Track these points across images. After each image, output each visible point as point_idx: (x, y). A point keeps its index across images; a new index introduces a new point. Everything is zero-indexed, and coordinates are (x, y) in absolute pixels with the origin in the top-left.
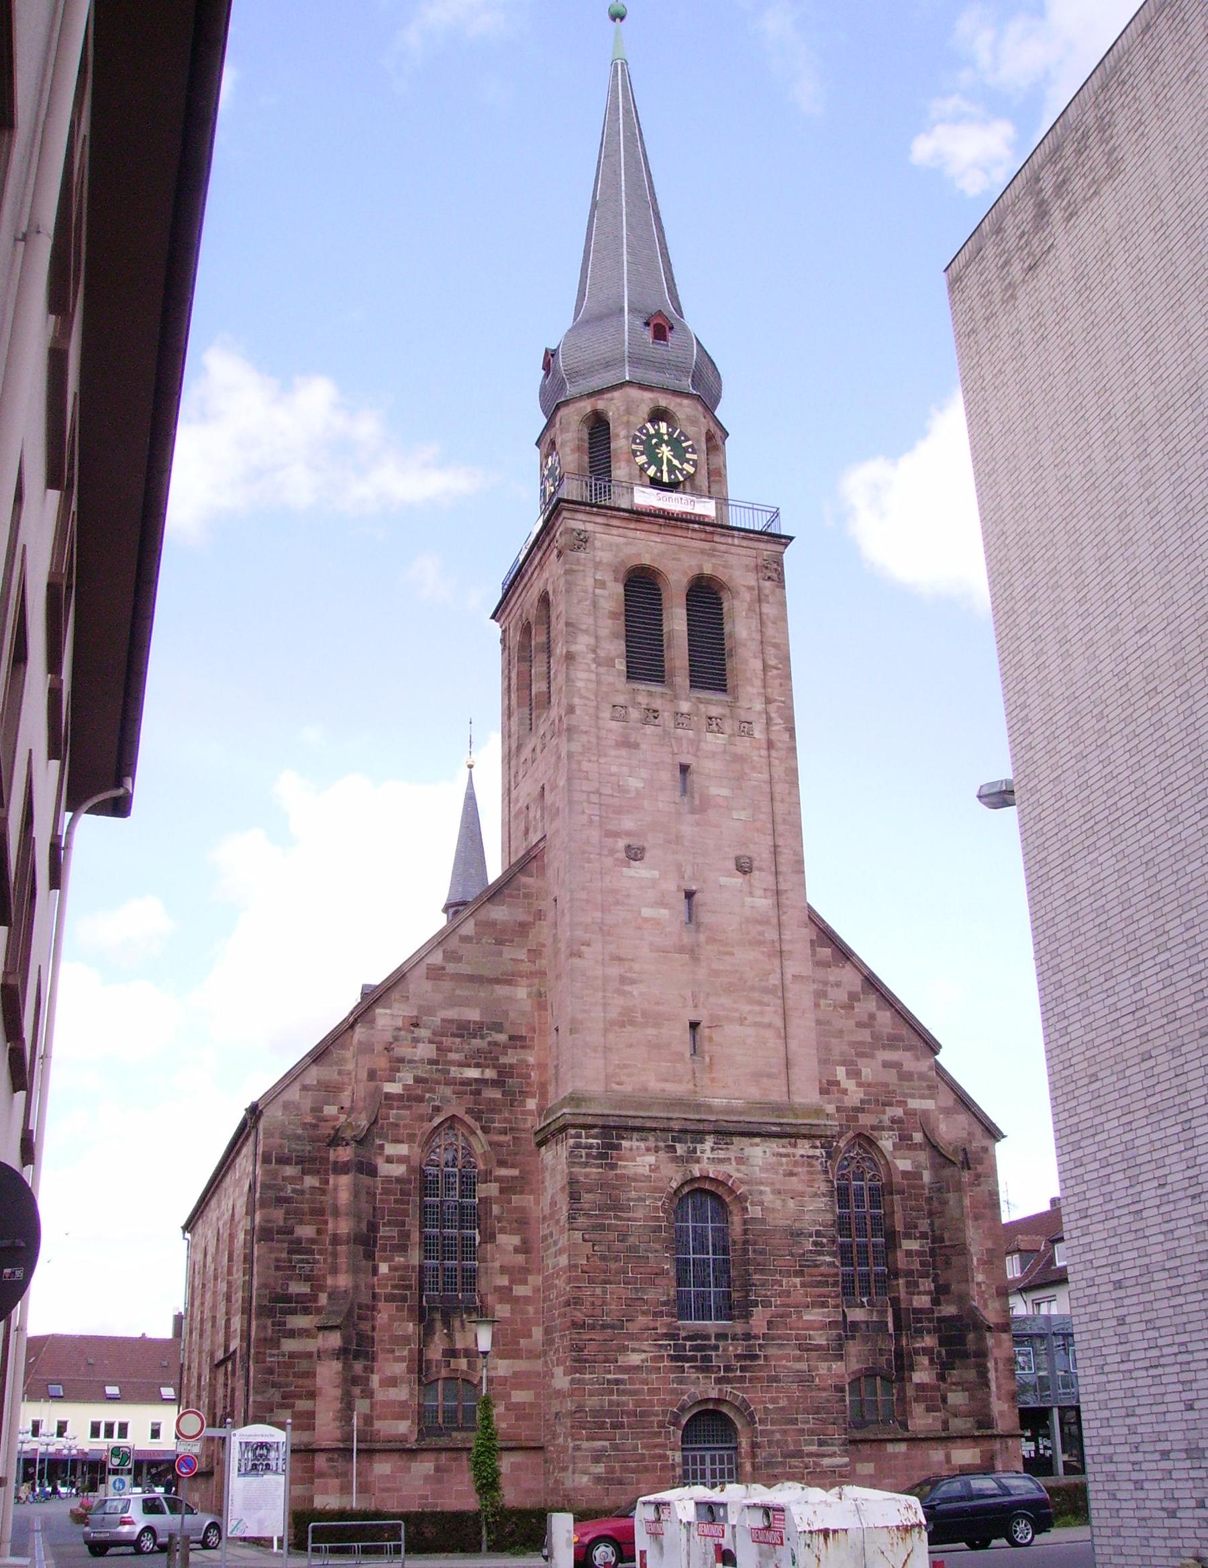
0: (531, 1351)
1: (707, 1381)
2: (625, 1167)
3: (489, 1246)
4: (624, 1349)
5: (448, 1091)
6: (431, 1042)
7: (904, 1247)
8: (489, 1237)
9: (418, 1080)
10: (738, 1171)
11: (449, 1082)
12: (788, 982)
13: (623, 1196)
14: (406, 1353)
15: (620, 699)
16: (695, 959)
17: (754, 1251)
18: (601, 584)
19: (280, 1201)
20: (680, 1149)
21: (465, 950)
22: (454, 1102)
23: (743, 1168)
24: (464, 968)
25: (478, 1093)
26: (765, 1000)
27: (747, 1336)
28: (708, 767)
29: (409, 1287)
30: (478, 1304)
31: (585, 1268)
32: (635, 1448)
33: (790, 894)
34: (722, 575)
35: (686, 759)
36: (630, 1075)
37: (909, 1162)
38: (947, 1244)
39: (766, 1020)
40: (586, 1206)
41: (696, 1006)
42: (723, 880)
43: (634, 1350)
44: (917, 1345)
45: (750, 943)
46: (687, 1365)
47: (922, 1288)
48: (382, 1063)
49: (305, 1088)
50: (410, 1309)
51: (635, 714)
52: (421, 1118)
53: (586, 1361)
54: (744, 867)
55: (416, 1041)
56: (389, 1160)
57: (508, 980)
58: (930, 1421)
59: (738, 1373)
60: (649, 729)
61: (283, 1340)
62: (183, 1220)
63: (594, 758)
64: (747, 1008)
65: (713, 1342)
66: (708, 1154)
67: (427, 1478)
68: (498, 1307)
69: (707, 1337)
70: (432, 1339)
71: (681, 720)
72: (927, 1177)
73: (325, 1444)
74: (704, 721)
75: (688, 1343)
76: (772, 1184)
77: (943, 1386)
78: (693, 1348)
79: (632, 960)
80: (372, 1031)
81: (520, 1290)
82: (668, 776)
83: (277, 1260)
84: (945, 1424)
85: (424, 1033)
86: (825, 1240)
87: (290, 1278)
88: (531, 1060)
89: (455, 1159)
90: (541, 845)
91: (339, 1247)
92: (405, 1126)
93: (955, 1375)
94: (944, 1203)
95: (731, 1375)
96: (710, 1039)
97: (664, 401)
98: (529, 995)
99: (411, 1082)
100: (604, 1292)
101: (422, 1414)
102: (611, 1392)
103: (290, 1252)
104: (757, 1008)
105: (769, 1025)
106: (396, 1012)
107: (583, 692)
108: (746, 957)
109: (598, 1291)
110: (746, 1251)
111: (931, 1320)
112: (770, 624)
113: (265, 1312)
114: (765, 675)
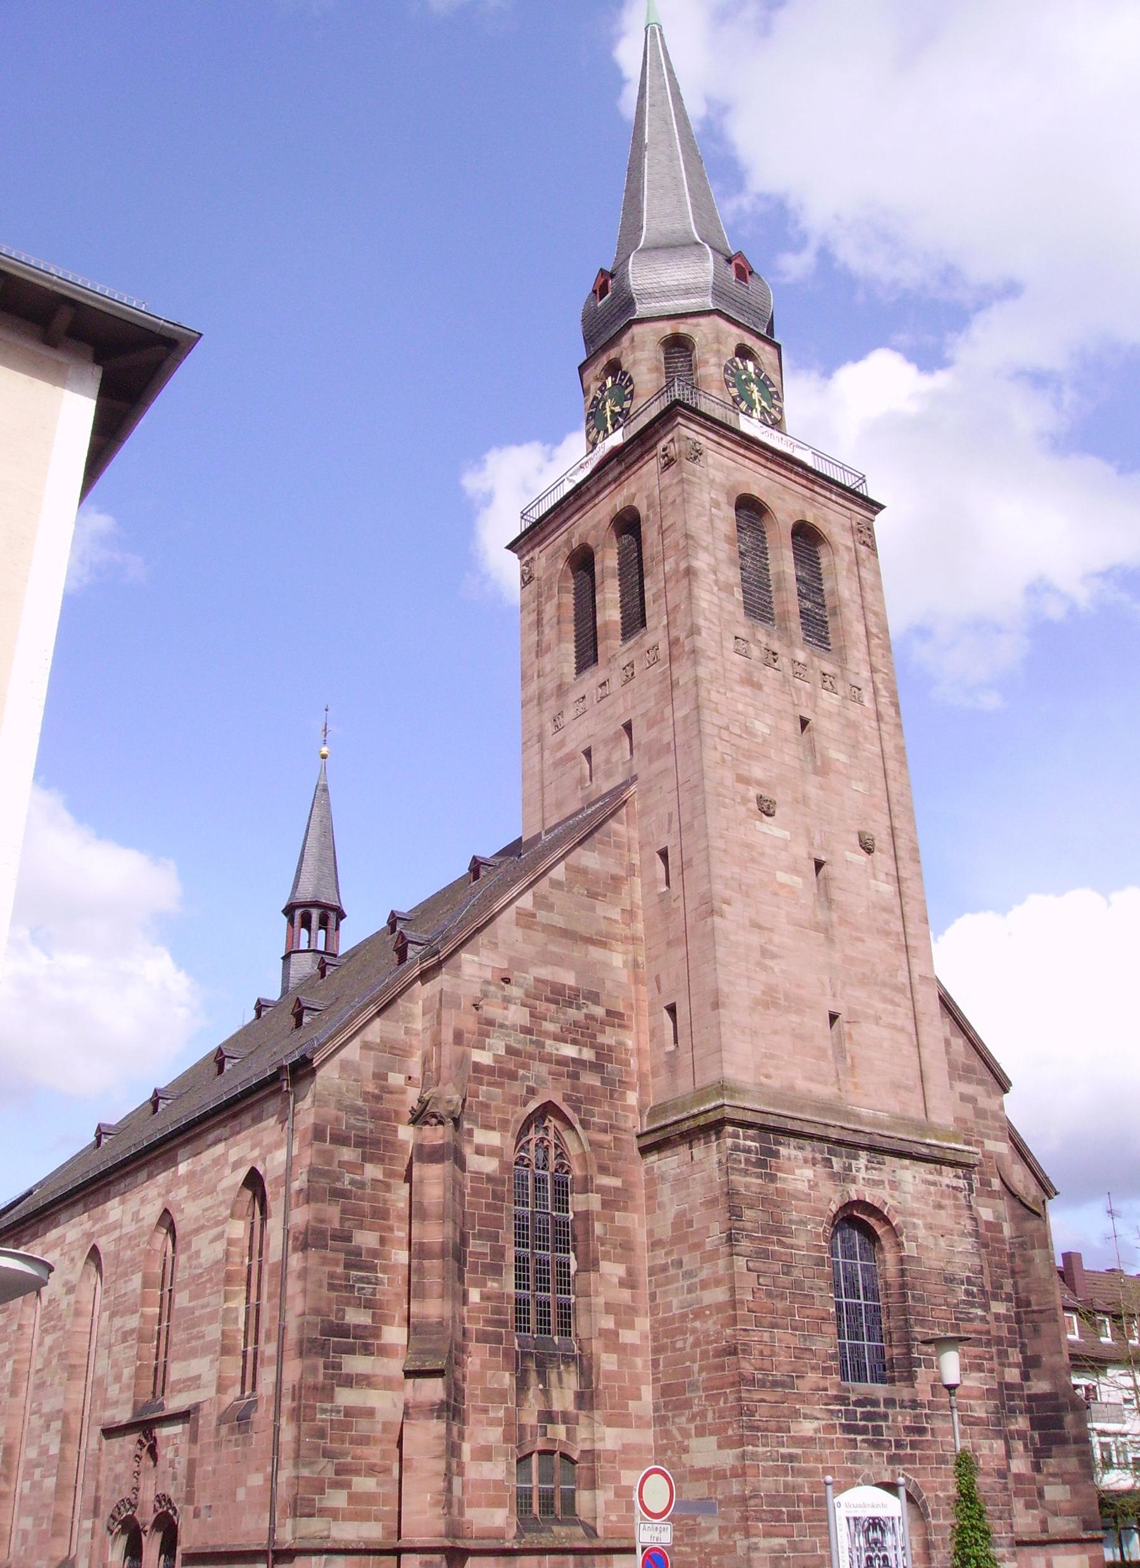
0: (639, 1418)
1: (880, 1460)
2: (784, 1180)
3: (593, 1275)
4: (796, 1414)
5: (542, 1069)
6: (524, 1005)
7: (993, 1310)
8: (590, 1264)
9: (510, 1050)
10: (892, 1196)
11: (545, 1059)
12: (916, 981)
13: (785, 1218)
14: (501, 1414)
15: (742, 632)
16: (830, 940)
17: (913, 1297)
18: (716, 504)
19: (338, 1194)
21: (556, 897)
22: (550, 1084)
23: (896, 1194)
24: (558, 921)
25: (575, 1076)
26: (896, 999)
27: (915, 1404)
28: (824, 725)
29: (503, 1323)
30: (577, 1352)
31: (751, 1305)
32: (814, 1549)
33: (909, 883)
34: (820, 525)
35: (807, 715)
36: (777, 1068)
37: (990, 1211)
38: (1035, 1308)
39: (899, 1023)
40: (749, 1225)
41: (834, 996)
42: (849, 856)
43: (806, 1417)
44: (1012, 1427)
45: (878, 931)
46: (859, 1438)
47: (1011, 1360)
48: (469, 1023)
49: (366, 1046)
50: (506, 1354)
51: (756, 652)
52: (513, 1100)
53: (758, 1429)
55: (507, 1000)
56: (479, 1151)
57: (601, 941)
58: (1030, 1520)
59: (909, 1451)
60: (770, 672)
61: (337, 1389)
63: (722, 690)
64: (880, 1006)
65: (882, 1409)
66: (863, 1174)
68: (604, 1356)
69: (875, 1403)
70: (526, 1396)
71: (799, 669)
72: (1007, 1230)
73: (419, 1541)
74: (819, 676)
75: (859, 1410)
76: (924, 1216)
77: (1038, 1477)
78: (867, 1416)
79: (771, 930)
80: (459, 981)
81: (628, 1337)
82: (790, 727)
83: (332, 1276)
84: (1044, 1522)
85: (515, 991)
86: (975, 1289)
87: (348, 1304)
88: (630, 1044)
89: (546, 1159)
91: (426, 1263)
93: (1051, 1464)
94: (1029, 1260)
95: (902, 1452)
96: (850, 1036)
97: (750, 341)
98: (625, 962)
99: (503, 1053)
100: (772, 1338)
101: (523, 1499)
102: (785, 1472)
103: (348, 1266)
104: (890, 1007)
105: (902, 1030)
106: (485, 961)
107: (707, 614)
108: (876, 946)
109: (766, 1337)
110: (904, 1296)
111: (1021, 1398)
112: (868, 590)
113: (307, 1348)
114: (868, 642)
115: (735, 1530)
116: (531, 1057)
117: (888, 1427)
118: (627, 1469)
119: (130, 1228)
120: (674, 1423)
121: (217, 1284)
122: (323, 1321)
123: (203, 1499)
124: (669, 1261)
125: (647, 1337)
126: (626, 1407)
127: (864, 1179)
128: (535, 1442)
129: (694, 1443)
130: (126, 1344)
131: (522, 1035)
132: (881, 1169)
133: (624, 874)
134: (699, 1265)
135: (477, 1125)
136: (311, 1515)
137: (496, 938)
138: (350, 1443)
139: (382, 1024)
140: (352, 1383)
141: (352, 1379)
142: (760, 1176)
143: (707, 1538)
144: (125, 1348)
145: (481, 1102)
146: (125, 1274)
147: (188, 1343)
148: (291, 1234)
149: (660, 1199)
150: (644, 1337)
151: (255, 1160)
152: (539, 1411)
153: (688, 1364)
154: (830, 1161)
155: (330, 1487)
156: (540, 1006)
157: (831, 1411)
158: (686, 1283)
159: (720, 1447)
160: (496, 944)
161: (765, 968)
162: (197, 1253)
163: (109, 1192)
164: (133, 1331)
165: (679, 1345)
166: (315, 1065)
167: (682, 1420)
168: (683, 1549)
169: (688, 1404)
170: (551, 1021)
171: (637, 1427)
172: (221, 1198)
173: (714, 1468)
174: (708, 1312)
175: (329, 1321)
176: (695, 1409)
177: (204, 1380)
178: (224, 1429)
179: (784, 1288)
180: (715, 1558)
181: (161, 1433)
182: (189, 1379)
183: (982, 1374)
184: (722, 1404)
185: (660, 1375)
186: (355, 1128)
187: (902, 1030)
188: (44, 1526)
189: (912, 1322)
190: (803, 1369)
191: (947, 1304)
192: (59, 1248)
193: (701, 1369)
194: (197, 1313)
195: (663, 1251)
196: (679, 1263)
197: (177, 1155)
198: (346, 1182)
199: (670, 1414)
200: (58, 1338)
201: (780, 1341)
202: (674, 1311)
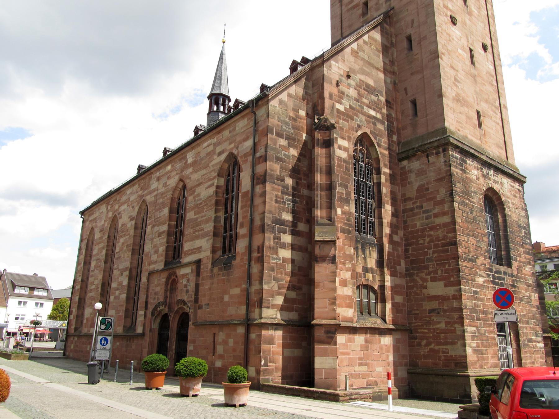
0: (400, 273)
2: (469, 173)
5: (362, 117)
6: (355, 89)
14: (350, 266)
16: (475, 80)
20: (485, 171)
21: (366, 48)
25: (375, 124)
26: (496, 112)
27: (512, 276)
41: (478, 104)
43: (480, 276)
49: (289, 95)
54: (485, 48)
55: (349, 86)
56: (340, 148)
61: (279, 249)
62: (82, 209)
64: (492, 113)
67: (361, 346)
75: (496, 275)
83: (276, 196)
85: (351, 81)
87: (284, 210)
88: (394, 115)
90: (392, 11)
92: (347, 131)
98: (391, 81)
100: (468, 240)
103: (283, 193)
104: (494, 114)
106: (340, 66)
115: (455, 322)
116: (359, 112)
117: (505, 283)
118: (396, 295)
119: (162, 190)
120: (417, 276)
121: (210, 206)
122: (273, 217)
123: (203, 301)
124: (415, 206)
125: (402, 239)
126: (396, 268)
127: (493, 179)
128: (361, 280)
129: (430, 284)
130: (160, 238)
131: (355, 102)
132: (498, 177)
133: (389, 46)
134: (432, 207)
135: (339, 136)
136: (268, 307)
137: (344, 58)
138: (285, 275)
139: (296, 87)
140: (285, 247)
141: (285, 245)
142: (461, 170)
143: (438, 326)
144: (160, 239)
145: (340, 127)
146: (160, 209)
147: (194, 233)
148: (255, 177)
149: (409, 180)
150: (401, 239)
151: (232, 149)
152: (362, 267)
153: (426, 250)
154: (482, 169)
155: (276, 295)
156: (362, 91)
157: (487, 274)
158: (425, 215)
159: (446, 286)
160: (344, 61)
161: (456, 86)
162: (199, 195)
163: (151, 177)
164: (164, 232)
165: (421, 242)
166: (269, 98)
167: (423, 275)
168: (423, 330)
169: (427, 267)
170: (365, 99)
171: (400, 277)
172: (212, 168)
173: (442, 295)
174: (438, 227)
175: (276, 217)
176: (431, 270)
177: (203, 248)
178: (216, 270)
179: (471, 219)
180: (443, 335)
181: (179, 273)
182: (194, 249)
183: (531, 267)
184: (447, 267)
185: (410, 256)
186: (285, 130)
187: (498, 124)
188: (121, 314)
189: (510, 241)
190: (478, 255)
191: (519, 236)
192: (127, 204)
193: (434, 252)
194: (199, 220)
195: (411, 202)
196: (421, 207)
197: (187, 155)
198: (282, 155)
199: (415, 272)
200: (126, 239)
201: (471, 241)
202: (418, 227)
